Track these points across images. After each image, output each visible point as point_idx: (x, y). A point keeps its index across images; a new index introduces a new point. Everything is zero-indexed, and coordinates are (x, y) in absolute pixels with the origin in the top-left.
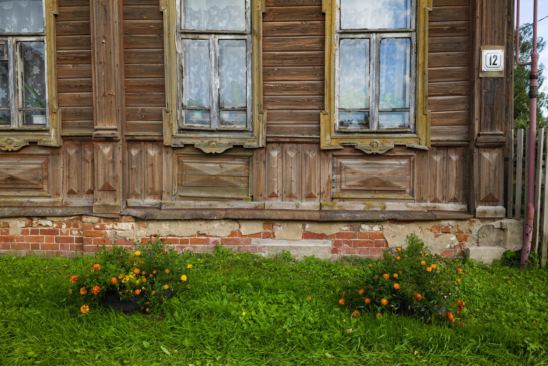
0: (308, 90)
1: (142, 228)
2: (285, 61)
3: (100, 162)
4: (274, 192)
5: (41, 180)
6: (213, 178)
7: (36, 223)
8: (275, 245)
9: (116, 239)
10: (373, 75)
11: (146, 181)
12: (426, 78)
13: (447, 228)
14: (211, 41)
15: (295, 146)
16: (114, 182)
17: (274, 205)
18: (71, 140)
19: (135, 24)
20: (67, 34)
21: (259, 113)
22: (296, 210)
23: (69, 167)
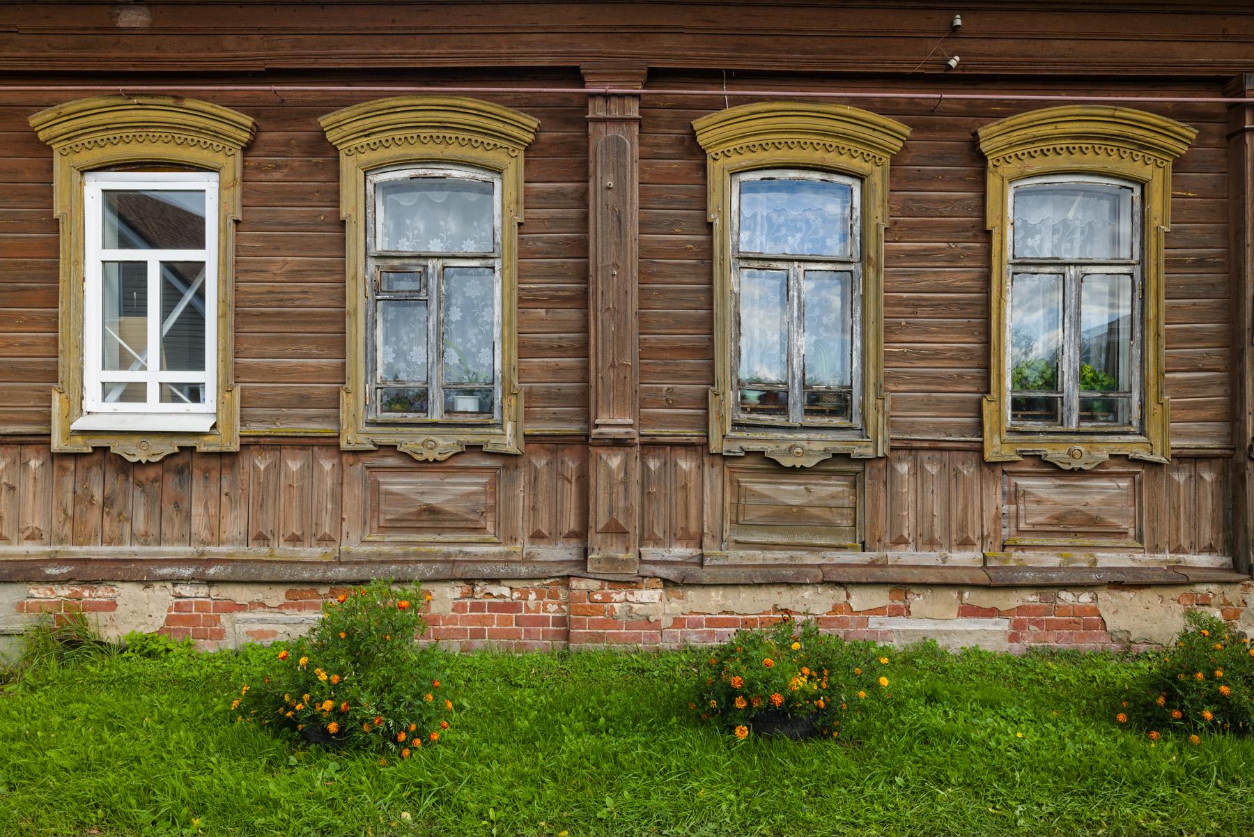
0: (959, 359)
1: (673, 599)
2: (919, 310)
3: (602, 483)
4: (902, 536)
5: (483, 513)
6: (794, 510)
7: (482, 591)
8: (910, 628)
9: (629, 620)
10: (1070, 336)
11: (674, 515)
12: (1162, 342)
13: (1205, 597)
14: (791, 273)
15: (937, 455)
16: (626, 518)
17: (903, 558)
18: (540, 442)
19: (660, 242)
20: (537, 256)
21: (877, 398)
22: (943, 567)
23: (534, 490)
